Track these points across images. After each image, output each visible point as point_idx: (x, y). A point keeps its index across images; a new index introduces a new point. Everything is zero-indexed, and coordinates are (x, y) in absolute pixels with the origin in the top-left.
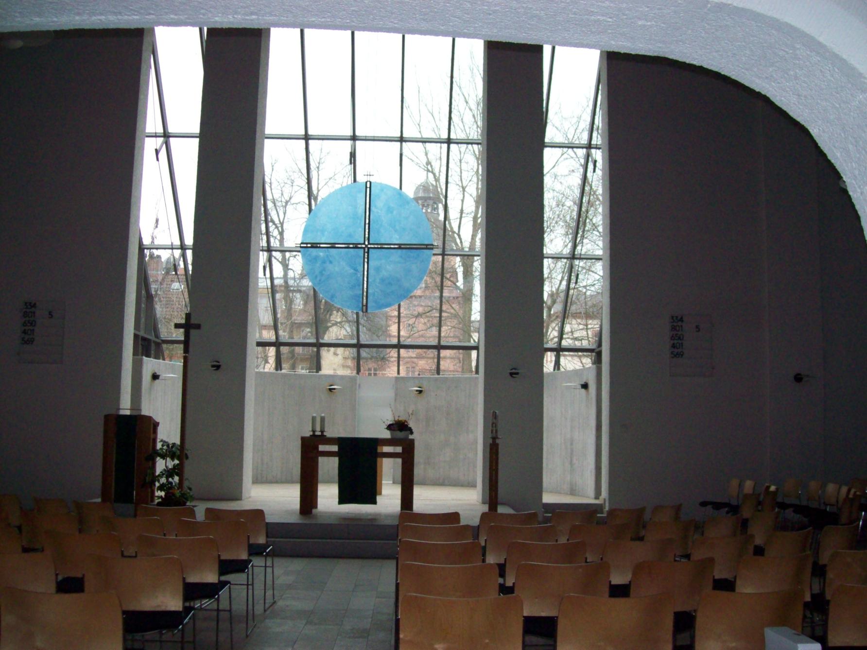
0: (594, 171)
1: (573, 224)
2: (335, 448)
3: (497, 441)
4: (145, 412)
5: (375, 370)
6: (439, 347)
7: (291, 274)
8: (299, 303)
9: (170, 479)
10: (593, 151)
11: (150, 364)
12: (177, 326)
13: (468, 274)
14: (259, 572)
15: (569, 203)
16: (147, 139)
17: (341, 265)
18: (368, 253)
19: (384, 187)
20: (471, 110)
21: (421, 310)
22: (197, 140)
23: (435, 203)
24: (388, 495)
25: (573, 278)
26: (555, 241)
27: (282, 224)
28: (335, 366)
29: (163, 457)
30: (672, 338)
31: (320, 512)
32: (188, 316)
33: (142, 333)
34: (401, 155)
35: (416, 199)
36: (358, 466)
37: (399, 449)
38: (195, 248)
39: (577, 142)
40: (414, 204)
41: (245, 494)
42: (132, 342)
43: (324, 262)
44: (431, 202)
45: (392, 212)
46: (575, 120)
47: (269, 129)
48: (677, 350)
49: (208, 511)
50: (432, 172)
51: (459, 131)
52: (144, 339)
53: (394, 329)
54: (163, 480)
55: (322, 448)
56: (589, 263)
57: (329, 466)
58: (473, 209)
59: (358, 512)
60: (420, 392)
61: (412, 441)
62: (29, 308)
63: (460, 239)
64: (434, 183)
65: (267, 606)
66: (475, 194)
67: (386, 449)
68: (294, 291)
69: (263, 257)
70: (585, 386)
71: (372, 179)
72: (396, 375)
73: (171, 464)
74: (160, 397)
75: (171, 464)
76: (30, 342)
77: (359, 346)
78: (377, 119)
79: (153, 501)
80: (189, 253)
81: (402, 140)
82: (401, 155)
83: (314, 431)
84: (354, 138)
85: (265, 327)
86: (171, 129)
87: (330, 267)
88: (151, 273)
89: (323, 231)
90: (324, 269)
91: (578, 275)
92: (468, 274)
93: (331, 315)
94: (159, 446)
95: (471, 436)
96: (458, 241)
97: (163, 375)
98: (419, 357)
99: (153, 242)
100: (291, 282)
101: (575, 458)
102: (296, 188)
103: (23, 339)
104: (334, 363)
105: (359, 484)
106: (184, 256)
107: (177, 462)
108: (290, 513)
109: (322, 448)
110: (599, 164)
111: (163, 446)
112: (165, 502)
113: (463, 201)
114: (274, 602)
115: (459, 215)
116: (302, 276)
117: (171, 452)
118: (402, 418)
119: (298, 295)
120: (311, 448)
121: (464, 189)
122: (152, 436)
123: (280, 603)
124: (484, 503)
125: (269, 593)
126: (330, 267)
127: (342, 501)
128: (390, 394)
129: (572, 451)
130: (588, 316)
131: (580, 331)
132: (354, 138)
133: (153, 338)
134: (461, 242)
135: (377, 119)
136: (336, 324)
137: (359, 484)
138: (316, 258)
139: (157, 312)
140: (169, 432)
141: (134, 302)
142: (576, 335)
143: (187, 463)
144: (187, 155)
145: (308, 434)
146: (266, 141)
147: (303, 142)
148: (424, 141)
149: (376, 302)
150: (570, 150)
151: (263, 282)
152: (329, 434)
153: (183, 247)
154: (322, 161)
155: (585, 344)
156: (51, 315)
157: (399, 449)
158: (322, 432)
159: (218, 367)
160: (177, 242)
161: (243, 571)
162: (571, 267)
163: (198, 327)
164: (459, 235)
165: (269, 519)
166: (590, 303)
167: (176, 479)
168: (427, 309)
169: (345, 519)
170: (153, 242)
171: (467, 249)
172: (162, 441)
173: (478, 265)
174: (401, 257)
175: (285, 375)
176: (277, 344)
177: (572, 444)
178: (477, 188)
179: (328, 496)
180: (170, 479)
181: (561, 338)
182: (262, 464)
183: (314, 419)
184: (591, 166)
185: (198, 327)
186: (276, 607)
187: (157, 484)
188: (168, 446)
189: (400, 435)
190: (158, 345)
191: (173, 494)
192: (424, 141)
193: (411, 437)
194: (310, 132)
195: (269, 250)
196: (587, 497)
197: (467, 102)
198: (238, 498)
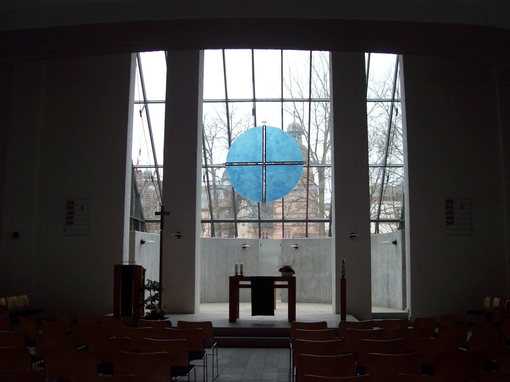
0: (397, 115)
1: (384, 146)
2: (249, 283)
3: (345, 277)
4: (137, 263)
5: (267, 234)
6: (307, 221)
7: (217, 179)
8: (222, 195)
9: (153, 302)
10: (396, 103)
11: (139, 235)
12: (157, 213)
13: (322, 178)
14: (210, 359)
15: (380, 133)
16: (135, 105)
17: (249, 175)
18: (265, 167)
19: (274, 129)
20: (321, 80)
21: (293, 198)
22: (164, 104)
23: (299, 135)
24: (280, 309)
25: (386, 179)
26: (374, 157)
27: (211, 150)
28: (244, 232)
29: (149, 289)
30: (447, 213)
31: (241, 321)
32: (162, 208)
33: (134, 217)
34: (282, 109)
35: (289, 132)
36: (263, 294)
37: (286, 283)
38: (165, 167)
39: (383, 98)
40: (288, 135)
41: (196, 310)
42: (129, 223)
43: (240, 174)
44: (297, 134)
45: (278, 144)
46: (381, 84)
47: (205, 97)
48: (450, 221)
49: (180, 323)
50: (299, 118)
51: (295, 87)
52: (135, 220)
53: (279, 210)
54: (149, 303)
55: (241, 283)
56: (394, 169)
57: (245, 293)
58: (324, 138)
59: (262, 320)
60: (297, 248)
61: (295, 278)
62: (70, 206)
63: (317, 156)
64: (300, 124)
65: (214, 378)
66: (324, 130)
67: (278, 283)
68: (219, 189)
69: (203, 170)
70: (395, 243)
71: (267, 124)
72: (282, 238)
73: (153, 293)
74: (146, 253)
75: (153, 293)
76: (71, 223)
77: (259, 221)
78: (268, 88)
79: (143, 315)
80: (161, 171)
81: (282, 100)
82: (282, 109)
83: (237, 273)
84: (254, 100)
85: (204, 210)
86: (148, 99)
87: (243, 177)
88: (138, 180)
89: (238, 156)
90: (239, 178)
91: (388, 176)
92: (322, 178)
93: (241, 202)
94: (146, 283)
95: (327, 273)
96: (315, 157)
97: (147, 241)
98: (293, 226)
99: (138, 163)
100: (217, 184)
101: (390, 285)
102: (218, 129)
103: (67, 222)
104: (244, 231)
105: (263, 304)
106: (157, 172)
107: (157, 292)
108: (224, 321)
109: (241, 283)
110: (400, 111)
111: (149, 283)
112: (150, 316)
113: (317, 134)
114: (218, 376)
115: (315, 142)
116: (223, 180)
117: (153, 286)
118: (289, 264)
119: (222, 191)
120: (235, 283)
121: (318, 128)
122: (142, 277)
123: (222, 376)
124: (337, 313)
125: (215, 369)
126: (243, 177)
127: (254, 314)
128: (279, 249)
129: (388, 281)
130: (394, 199)
131: (389, 209)
132: (254, 100)
133: (140, 219)
134: (317, 158)
135: (268, 88)
136: (244, 207)
137: (263, 304)
138: (235, 172)
139: (142, 205)
140: (152, 274)
141: (130, 199)
142: (387, 211)
143: (163, 292)
144: (158, 114)
145: (233, 275)
146: (204, 103)
147: (225, 104)
148: (294, 101)
149: (270, 196)
150: (380, 103)
151: (203, 184)
152: (246, 274)
153: (156, 166)
154: (233, 113)
155: (393, 217)
156: (82, 208)
157: (286, 283)
158: (241, 273)
159: (179, 236)
160: (153, 163)
161: (201, 358)
162: (384, 172)
163: (168, 214)
164: (316, 154)
165: (214, 325)
166: (395, 192)
167: (157, 302)
168: (297, 198)
169: (256, 325)
170: (138, 163)
171: (320, 163)
172: (148, 280)
173: (328, 172)
174: (284, 169)
175: (217, 240)
176: (212, 221)
177: (388, 277)
178: (326, 126)
179: (245, 310)
180: (153, 302)
181: (379, 214)
182: (205, 292)
183: (236, 266)
184: (394, 112)
185: (168, 214)
186: (219, 378)
187: (146, 305)
188: (152, 283)
189: (286, 274)
190: (143, 223)
191: (156, 312)
192: (294, 101)
193: (293, 275)
194: (229, 98)
195: (206, 167)
196: (398, 309)
197: (318, 76)
198: (191, 312)
